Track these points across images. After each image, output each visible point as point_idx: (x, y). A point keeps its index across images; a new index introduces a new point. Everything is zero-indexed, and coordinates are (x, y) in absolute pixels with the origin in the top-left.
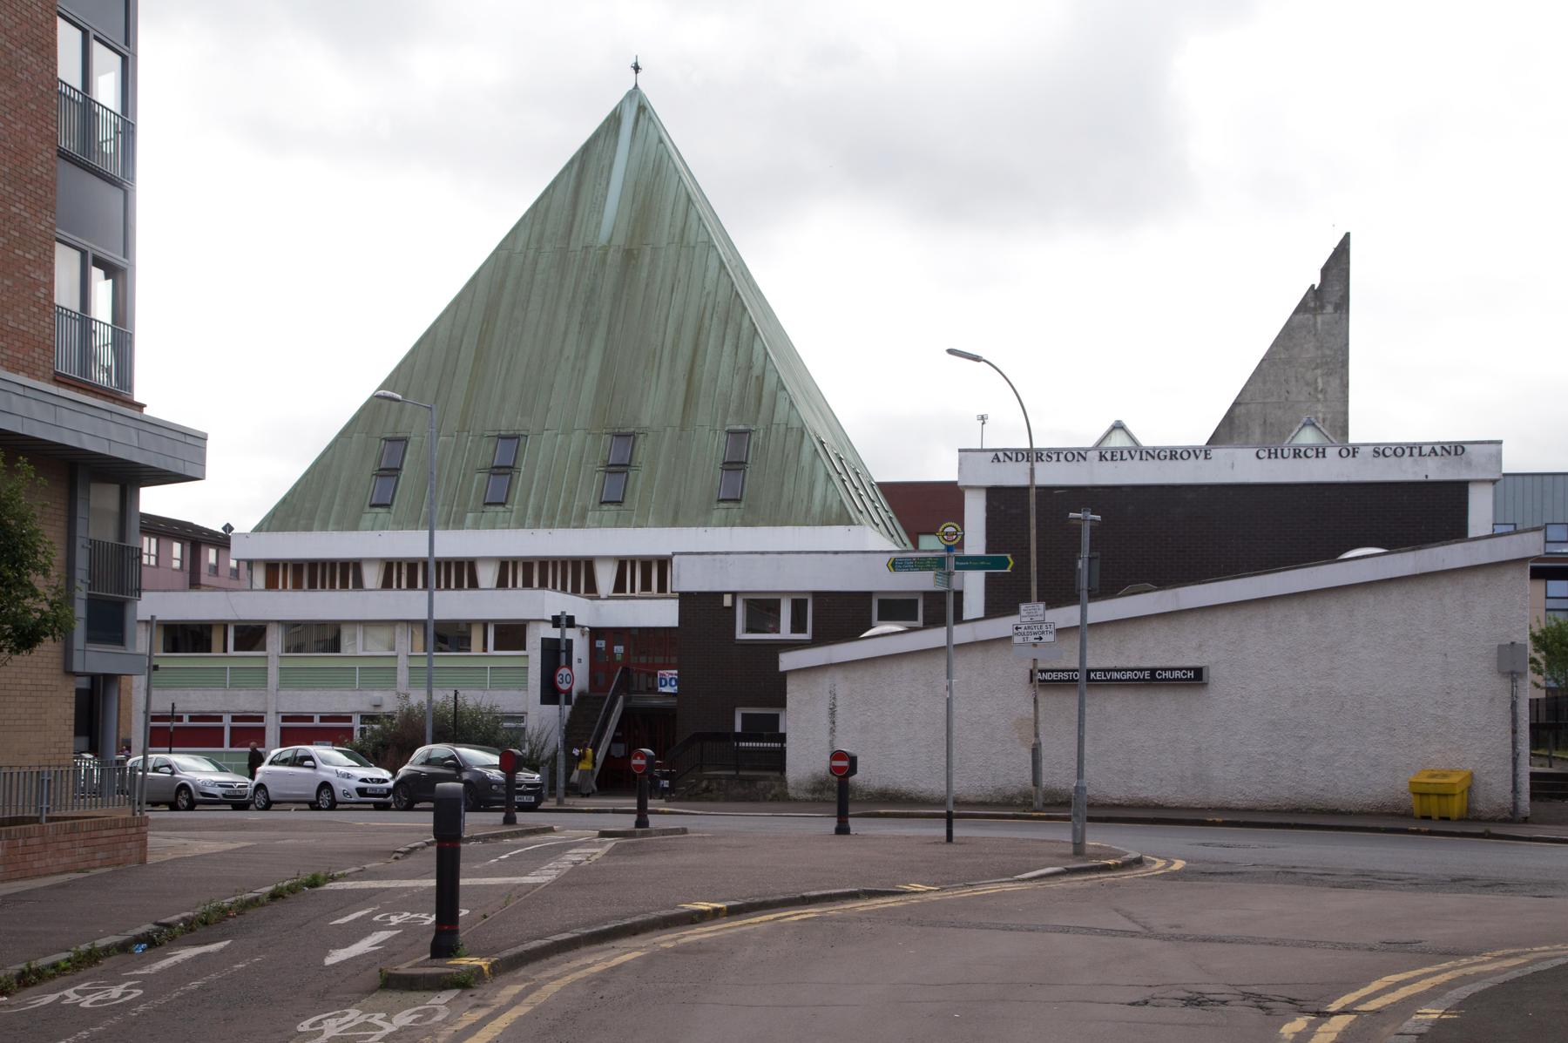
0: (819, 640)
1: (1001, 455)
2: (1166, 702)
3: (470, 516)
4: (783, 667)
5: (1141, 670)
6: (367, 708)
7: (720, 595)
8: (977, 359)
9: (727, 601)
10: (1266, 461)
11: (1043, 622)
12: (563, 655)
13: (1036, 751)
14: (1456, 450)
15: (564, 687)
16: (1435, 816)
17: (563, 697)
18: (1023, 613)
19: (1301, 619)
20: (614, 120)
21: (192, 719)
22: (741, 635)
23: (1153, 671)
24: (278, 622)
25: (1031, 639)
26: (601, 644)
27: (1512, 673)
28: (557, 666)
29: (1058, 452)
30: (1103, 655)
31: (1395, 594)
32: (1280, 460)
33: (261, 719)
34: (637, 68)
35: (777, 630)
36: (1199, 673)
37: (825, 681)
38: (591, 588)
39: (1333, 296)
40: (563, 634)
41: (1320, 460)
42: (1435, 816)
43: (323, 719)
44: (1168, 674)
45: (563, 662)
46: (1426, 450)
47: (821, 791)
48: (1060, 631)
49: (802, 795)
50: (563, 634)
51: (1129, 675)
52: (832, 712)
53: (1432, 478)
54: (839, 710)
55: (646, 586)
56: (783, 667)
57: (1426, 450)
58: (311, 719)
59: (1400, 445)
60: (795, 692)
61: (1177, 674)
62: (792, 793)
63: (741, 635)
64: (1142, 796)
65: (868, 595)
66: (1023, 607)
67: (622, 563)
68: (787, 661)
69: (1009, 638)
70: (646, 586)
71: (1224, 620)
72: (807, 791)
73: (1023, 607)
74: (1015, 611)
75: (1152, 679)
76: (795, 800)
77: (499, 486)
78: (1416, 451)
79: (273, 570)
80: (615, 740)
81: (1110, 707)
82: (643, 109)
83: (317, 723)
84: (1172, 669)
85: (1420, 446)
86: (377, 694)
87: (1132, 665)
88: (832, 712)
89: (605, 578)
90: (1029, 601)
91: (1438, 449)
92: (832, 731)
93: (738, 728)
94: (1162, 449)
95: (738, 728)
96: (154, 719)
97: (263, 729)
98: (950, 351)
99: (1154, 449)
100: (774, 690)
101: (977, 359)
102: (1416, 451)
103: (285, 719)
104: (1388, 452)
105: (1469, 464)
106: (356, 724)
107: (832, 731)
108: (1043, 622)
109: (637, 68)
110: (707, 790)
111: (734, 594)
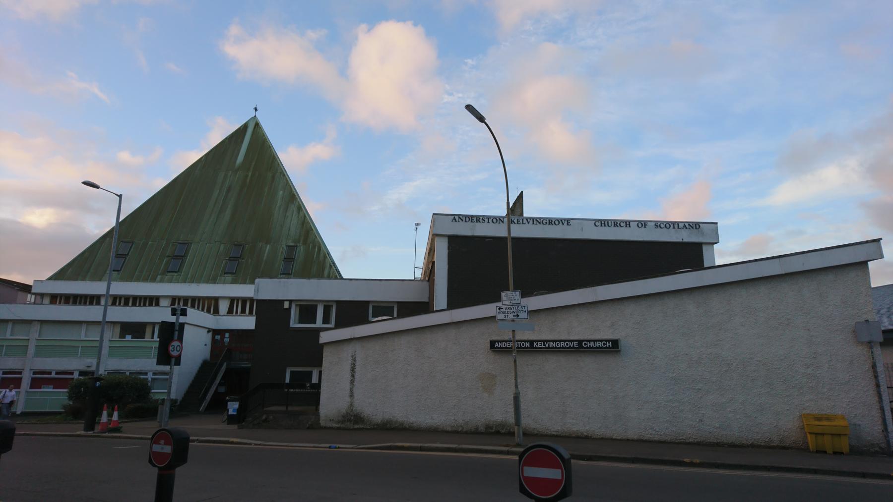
0: (339, 325)
1: (457, 218)
2: (588, 363)
3: (159, 277)
4: (322, 341)
5: (571, 341)
6: (83, 368)
7: (283, 301)
8: (481, 119)
9: (286, 305)
10: (600, 228)
11: (519, 304)
12: (176, 333)
13: (516, 399)
14: (695, 226)
15: (175, 353)
16: (830, 451)
17: (173, 360)
18: (504, 298)
19: (690, 305)
20: (244, 128)
21: (57, 373)
22: (294, 324)
23: (580, 342)
24: (38, 321)
25: (511, 316)
26: (218, 337)
27: (870, 342)
28: (172, 340)
29: (489, 217)
30: (542, 332)
31: (763, 289)
32: (607, 228)
33: (20, 373)
34: (256, 110)
35: (314, 321)
36: (615, 343)
37: (347, 351)
38: (216, 312)
39: (518, 211)
40: (177, 319)
41: (628, 228)
42: (830, 451)
43: (57, 373)
44: (592, 344)
45: (176, 337)
46: (681, 225)
47: (343, 422)
48: (531, 312)
49: (330, 424)
50: (177, 319)
51: (562, 344)
52: (353, 370)
53: (686, 240)
54: (358, 368)
55: (243, 311)
56: (322, 341)
57: (681, 225)
58: (50, 373)
59: (668, 222)
60: (328, 356)
61: (598, 344)
62: (322, 423)
63: (294, 324)
64: (575, 429)
65: (368, 303)
66: (503, 294)
67: (232, 300)
68: (324, 337)
69: (495, 317)
70: (243, 311)
71: (629, 309)
72: (339, 422)
73: (503, 294)
74: (498, 299)
75: (580, 348)
76: (326, 428)
77: (174, 265)
78: (676, 226)
79: (55, 298)
80: (220, 384)
81: (530, 365)
82: (257, 125)
83: (53, 375)
84: (594, 341)
85: (678, 223)
86: (89, 360)
87: (563, 338)
88: (353, 370)
89: (224, 307)
90: (507, 289)
91: (687, 225)
92: (352, 382)
93: (287, 380)
94: (545, 219)
95: (287, 380)
96: (35, 373)
97: (21, 378)
98: (469, 108)
99: (540, 218)
100: (313, 353)
101: (481, 119)
102: (676, 226)
103: (35, 373)
104: (662, 226)
105: (703, 234)
106: (76, 376)
107: (352, 382)
108: (519, 304)
109: (256, 110)
110: (266, 420)
111: (291, 301)
